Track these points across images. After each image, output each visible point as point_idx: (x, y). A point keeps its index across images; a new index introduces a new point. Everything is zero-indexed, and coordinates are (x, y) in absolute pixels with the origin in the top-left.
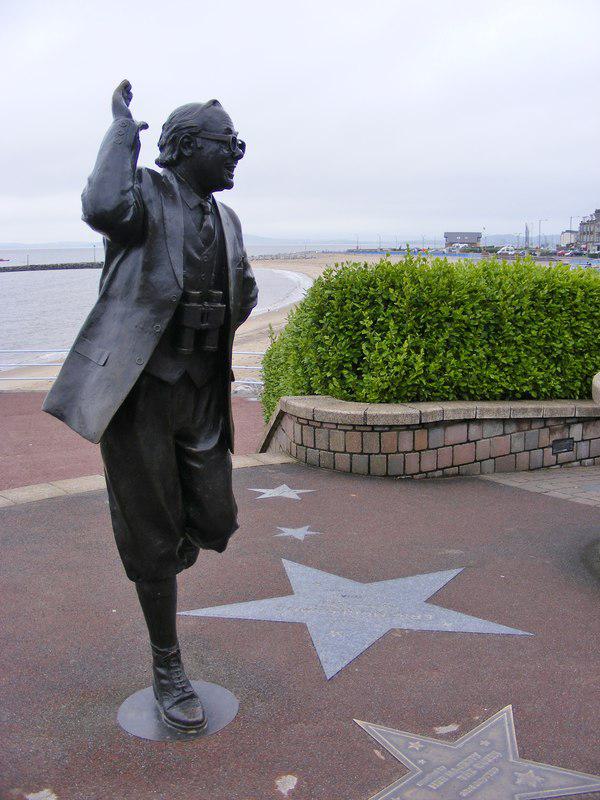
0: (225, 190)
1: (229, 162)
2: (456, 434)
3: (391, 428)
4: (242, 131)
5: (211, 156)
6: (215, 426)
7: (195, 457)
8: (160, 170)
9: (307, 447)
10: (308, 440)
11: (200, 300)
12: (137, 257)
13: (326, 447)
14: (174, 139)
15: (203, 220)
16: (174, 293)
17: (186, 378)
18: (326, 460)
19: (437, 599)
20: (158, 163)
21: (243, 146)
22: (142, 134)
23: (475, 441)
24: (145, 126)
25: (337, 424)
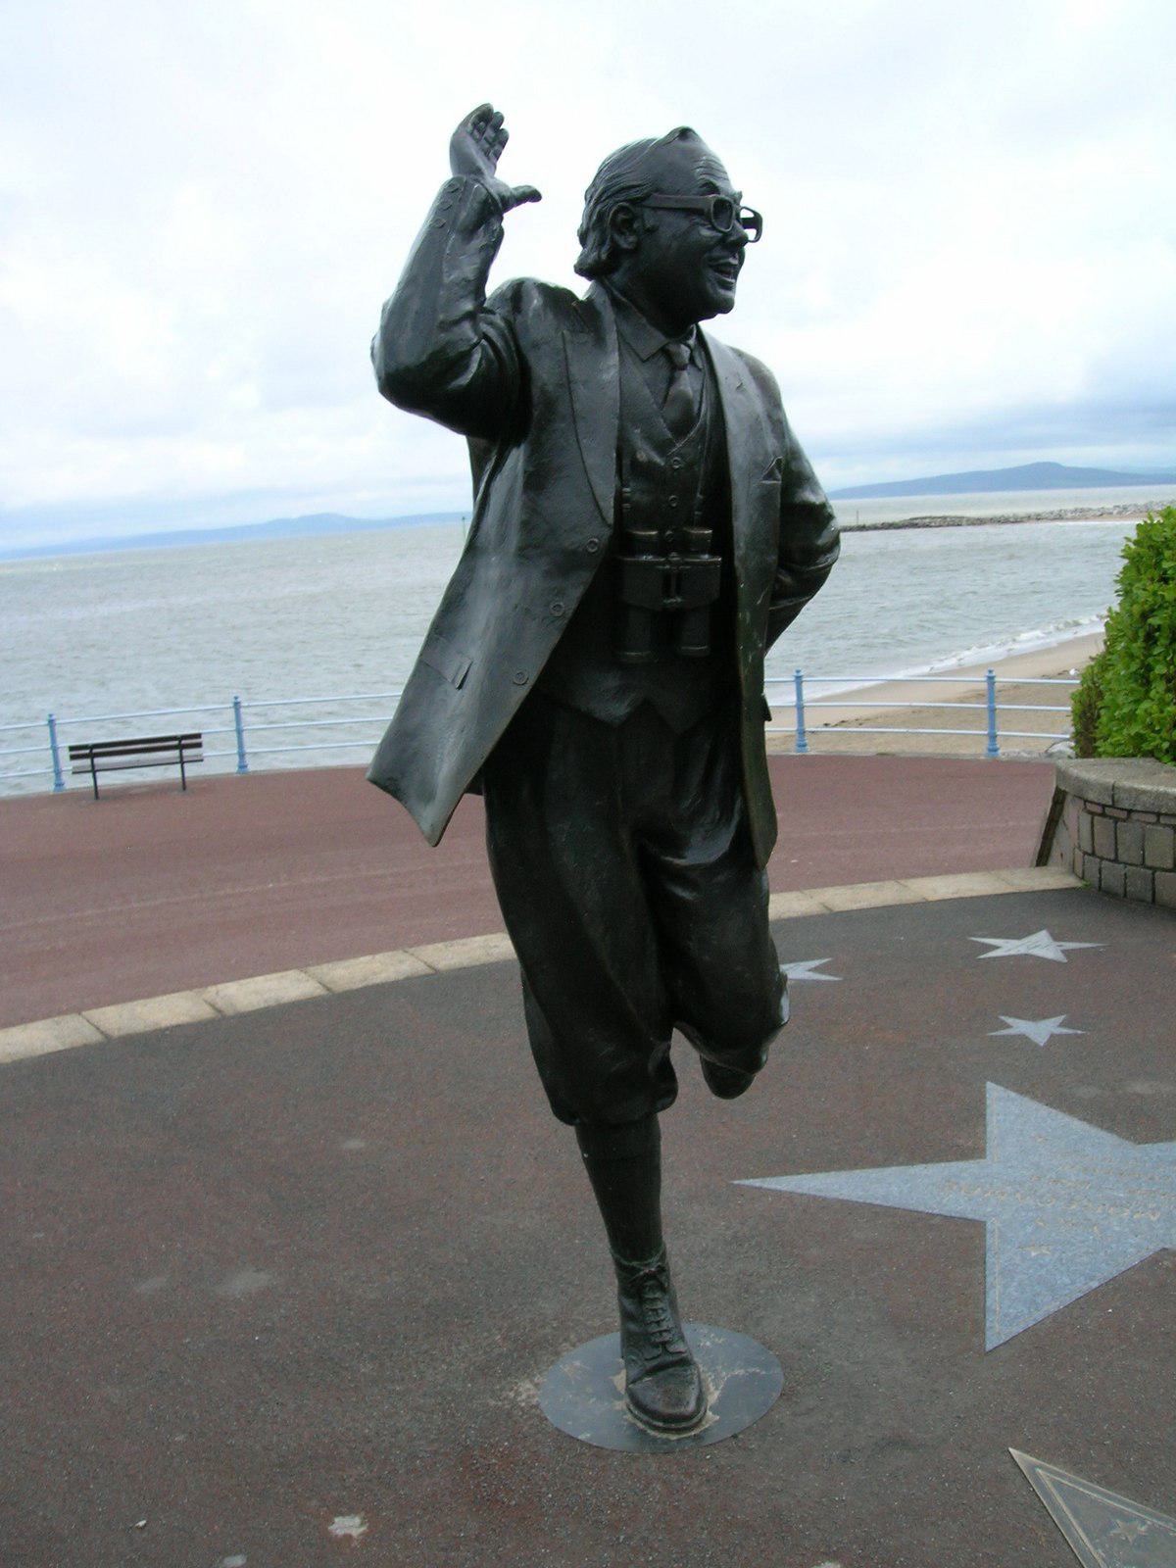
0: (719, 316)
1: (717, 253)
5: (675, 244)
6: (726, 810)
7: (681, 876)
9: (1102, 859)
10: (1105, 848)
11: (662, 548)
12: (517, 459)
13: (1138, 861)
14: (601, 217)
15: (672, 381)
16: (594, 535)
17: (644, 711)
18: (1138, 887)
20: (583, 269)
21: (755, 222)
22: (511, 220)
25: (1159, 815)
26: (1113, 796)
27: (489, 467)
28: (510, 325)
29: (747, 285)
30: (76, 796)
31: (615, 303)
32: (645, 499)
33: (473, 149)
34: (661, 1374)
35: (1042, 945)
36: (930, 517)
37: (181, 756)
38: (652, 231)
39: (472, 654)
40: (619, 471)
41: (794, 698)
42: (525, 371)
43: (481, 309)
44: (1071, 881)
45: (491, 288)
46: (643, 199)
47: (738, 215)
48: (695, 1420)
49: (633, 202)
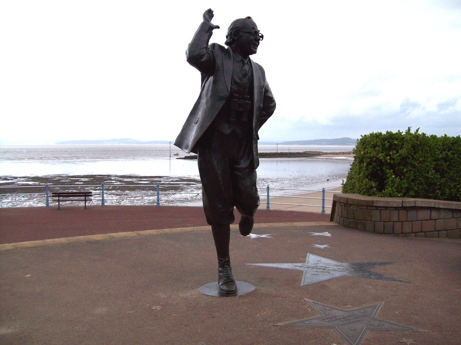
2: (423, 215)
3: (386, 208)
4: (261, 28)
8: (226, 47)
12: (211, 78)
15: (243, 66)
19: (328, 246)
20: (226, 43)
21: (262, 37)
22: (215, 31)
23: (435, 220)
24: (218, 27)
25: (358, 206)
26: (347, 201)
27: (205, 80)
28: (212, 52)
29: (259, 49)
30: (53, 209)
31: (233, 50)
32: (237, 89)
33: (207, 17)
34: (226, 284)
35: (327, 234)
36: (311, 152)
37: (85, 199)
38: (241, 36)
39: (200, 115)
40: (231, 83)
41: (266, 194)
42: (214, 60)
43: (207, 48)
44: (336, 224)
45: (210, 43)
46: (240, 30)
47: (259, 35)
48: (235, 292)
49: (238, 30)
